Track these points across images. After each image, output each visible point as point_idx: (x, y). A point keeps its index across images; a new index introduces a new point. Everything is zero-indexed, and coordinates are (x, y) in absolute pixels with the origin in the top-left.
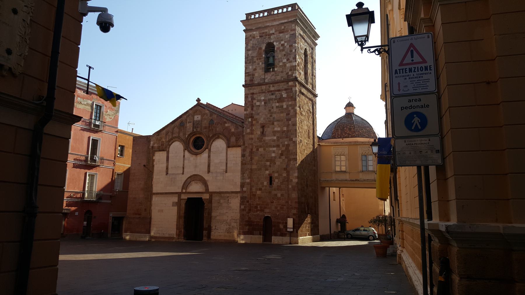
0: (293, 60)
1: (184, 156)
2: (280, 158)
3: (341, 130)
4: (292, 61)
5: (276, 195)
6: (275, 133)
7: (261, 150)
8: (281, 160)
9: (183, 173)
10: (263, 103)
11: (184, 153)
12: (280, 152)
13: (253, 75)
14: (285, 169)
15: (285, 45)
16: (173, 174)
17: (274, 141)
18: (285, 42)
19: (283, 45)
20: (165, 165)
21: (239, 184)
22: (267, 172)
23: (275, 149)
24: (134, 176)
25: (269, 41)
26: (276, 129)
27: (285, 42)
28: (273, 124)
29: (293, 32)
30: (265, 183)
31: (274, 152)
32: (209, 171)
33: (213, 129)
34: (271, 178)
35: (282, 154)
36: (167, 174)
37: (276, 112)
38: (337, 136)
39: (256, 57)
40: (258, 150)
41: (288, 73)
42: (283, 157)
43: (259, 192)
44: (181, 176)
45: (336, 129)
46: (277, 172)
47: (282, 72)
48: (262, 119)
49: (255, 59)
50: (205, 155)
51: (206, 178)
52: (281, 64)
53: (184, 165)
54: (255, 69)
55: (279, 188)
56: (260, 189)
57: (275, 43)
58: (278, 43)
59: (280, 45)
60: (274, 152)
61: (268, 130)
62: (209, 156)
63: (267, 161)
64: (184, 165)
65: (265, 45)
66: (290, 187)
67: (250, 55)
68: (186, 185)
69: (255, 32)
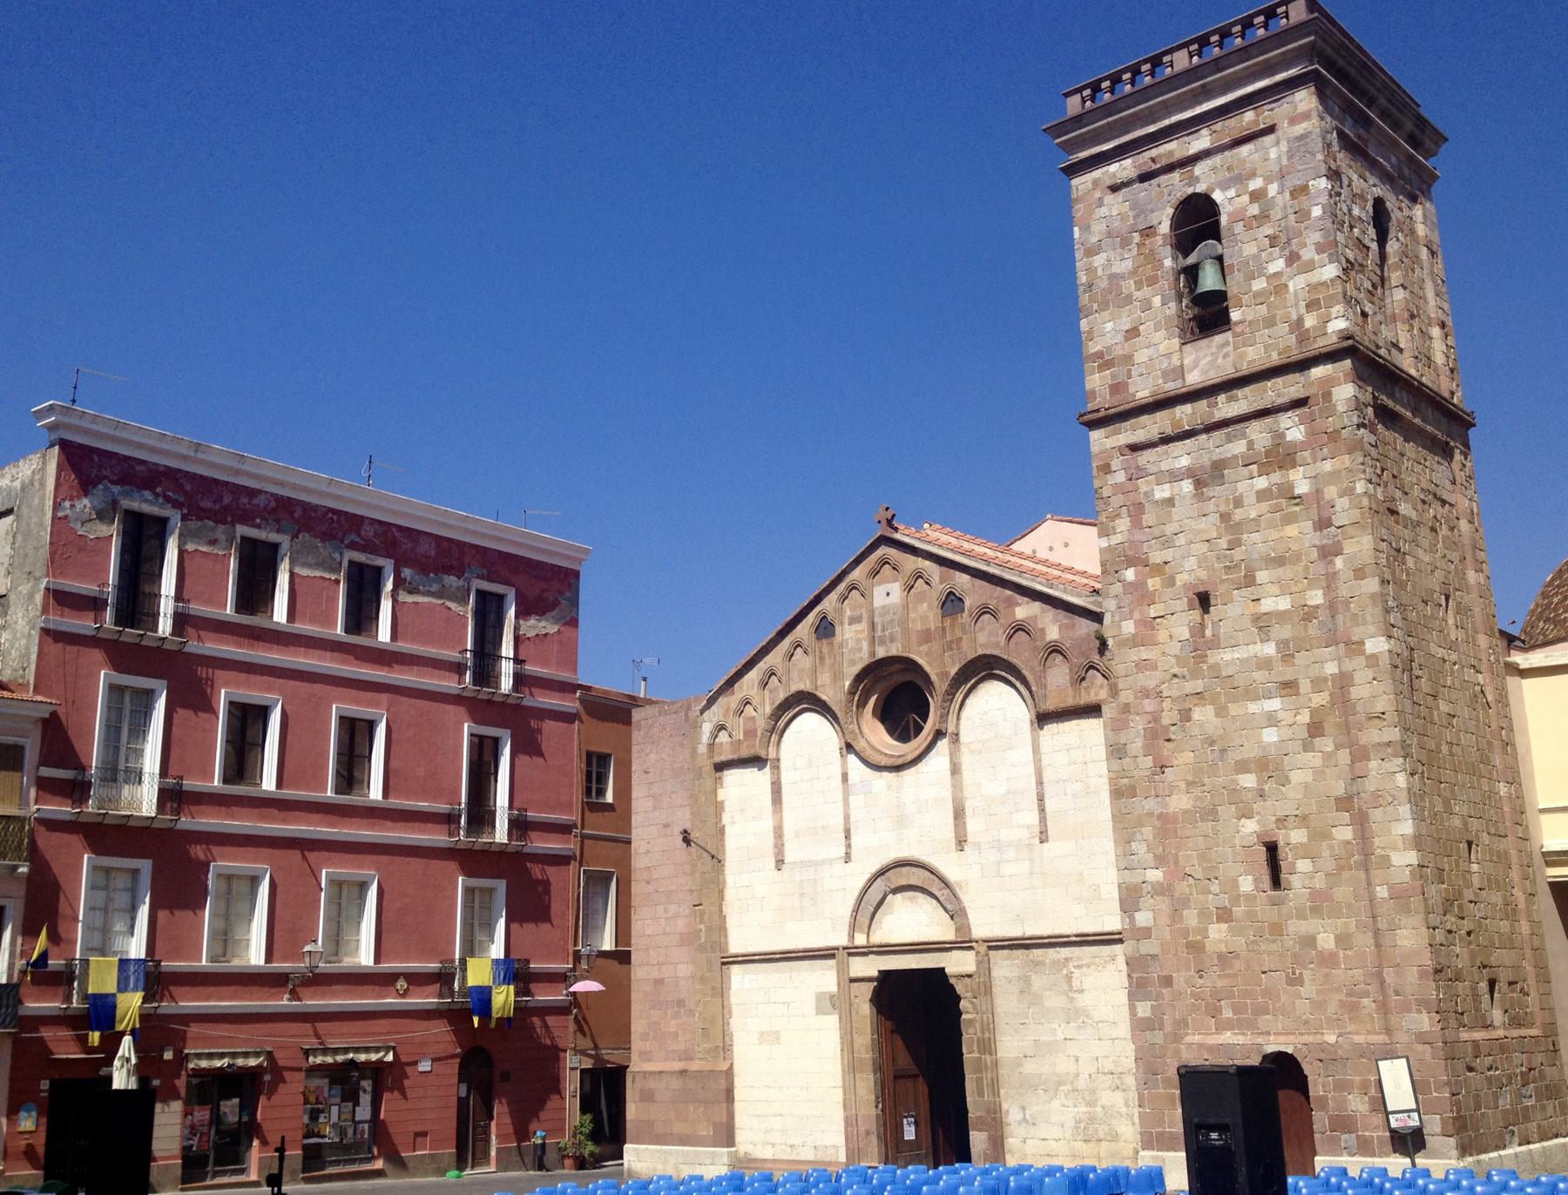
0: (1316, 257)
1: (845, 777)
2: (1308, 747)
4: (1312, 261)
5: (1310, 941)
6: (1263, 624)
7: (1203, 714)
8: (1315, 759)
9: (848, 858)
10: (1187, 486)
11: (844, 764)
12: (1304, 717)
13: (1128, 359)
14: (1344, 803)
16: (804, 864)
17: (1265, 664)
18: (1268, 180)
19: (1256, 196)
21: (1112, 894)
22: (1250, 826)
23: (1274, 704)
24: (648, 883)
25: (1190, 191)
26: (1267, 605)
27: (1268, 180)
28: (1250, 581)
29: (1304, 125)
30: (1246, 884)
31: (1272, 720)
32: (961, 843)
34: (1272, 849)
35: (1315, 729)
36: (780, 863)
37: (1256, 520)
39: (1134, 273)
40: (1186, 715)
41: (1300, 320)
43: (1217, 933)
44: (840, 867)
46: (1303, 820)
47: (1270, 322)
48: (1191, 563)
49: (1129, 285)
50: (939, 759)
51: (951, 874)
52: (1259, 285)
53: (847, 817)
54: (1133, 333)
55: (1320, 903)
56: (1224, 915)
57: (1217, 196)
58: (1232, 193)
59: (1246, 198)
60: (1272, 720)
61: (1231, 611)
62: (955, 770)
63: (1242, 767)
64: (847, 817)
65: (1170, 211)
66: (1382, 892)
67: (1100, 272)
68: (868, 907)
69: (1117, 164)
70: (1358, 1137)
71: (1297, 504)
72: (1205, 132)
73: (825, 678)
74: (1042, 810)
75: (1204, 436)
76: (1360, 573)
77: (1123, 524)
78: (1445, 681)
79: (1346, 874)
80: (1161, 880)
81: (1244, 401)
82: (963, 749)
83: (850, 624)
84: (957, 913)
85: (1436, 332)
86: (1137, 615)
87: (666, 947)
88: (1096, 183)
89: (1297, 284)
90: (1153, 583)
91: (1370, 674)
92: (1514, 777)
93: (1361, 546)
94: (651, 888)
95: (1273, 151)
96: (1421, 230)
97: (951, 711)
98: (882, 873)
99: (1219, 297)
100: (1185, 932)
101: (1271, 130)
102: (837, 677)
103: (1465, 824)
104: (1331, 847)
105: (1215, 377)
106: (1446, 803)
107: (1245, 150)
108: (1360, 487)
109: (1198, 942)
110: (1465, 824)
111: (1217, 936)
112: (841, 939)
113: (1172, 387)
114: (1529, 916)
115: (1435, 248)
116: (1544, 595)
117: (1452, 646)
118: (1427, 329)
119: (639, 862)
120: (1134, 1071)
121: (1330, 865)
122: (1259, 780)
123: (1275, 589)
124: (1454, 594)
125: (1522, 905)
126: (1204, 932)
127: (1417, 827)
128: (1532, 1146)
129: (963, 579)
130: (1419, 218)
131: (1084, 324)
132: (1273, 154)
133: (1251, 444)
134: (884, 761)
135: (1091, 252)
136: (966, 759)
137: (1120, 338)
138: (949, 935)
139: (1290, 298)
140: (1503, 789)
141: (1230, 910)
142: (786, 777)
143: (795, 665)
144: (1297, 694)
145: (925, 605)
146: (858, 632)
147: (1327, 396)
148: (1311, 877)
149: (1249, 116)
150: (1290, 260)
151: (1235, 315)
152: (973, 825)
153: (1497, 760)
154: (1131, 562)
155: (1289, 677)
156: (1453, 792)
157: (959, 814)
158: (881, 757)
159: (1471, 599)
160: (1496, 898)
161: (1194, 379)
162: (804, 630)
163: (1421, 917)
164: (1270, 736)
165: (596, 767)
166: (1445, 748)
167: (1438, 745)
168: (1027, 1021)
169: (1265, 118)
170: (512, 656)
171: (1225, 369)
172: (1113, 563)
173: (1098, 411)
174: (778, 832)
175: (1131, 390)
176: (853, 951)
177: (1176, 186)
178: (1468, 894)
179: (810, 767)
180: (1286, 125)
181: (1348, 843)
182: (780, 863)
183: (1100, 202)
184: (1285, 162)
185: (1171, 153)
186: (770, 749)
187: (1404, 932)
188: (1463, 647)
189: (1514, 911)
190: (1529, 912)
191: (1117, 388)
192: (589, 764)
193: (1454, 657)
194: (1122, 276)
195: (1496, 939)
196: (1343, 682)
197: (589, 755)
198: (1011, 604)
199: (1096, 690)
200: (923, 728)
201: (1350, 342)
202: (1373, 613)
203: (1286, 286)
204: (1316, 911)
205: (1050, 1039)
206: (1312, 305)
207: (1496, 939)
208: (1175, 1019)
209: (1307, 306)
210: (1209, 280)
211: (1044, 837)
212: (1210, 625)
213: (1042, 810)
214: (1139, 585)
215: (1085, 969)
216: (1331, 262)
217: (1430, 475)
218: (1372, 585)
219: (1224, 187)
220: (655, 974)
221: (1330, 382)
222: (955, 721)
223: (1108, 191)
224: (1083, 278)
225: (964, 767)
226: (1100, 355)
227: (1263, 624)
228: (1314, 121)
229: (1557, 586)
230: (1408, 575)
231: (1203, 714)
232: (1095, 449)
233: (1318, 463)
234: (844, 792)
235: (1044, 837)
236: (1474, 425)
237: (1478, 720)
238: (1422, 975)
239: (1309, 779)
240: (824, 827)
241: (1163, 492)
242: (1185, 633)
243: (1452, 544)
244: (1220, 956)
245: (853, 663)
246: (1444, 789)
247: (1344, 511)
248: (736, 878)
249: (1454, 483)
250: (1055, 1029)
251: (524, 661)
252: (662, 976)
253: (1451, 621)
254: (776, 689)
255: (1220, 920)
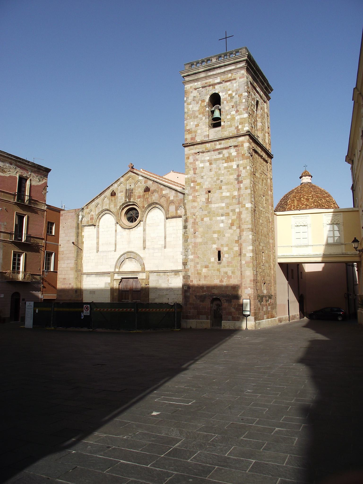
1: (116, 231)
2: (230, 228)
3: (298, 200)
5: (226, 273)
6: (222, 199)
7: (206, 219)
8: (231, 231)
9: (115, 251)
10: (208, 164)
11: (116, 228)
12: (230, 221)
13: (196, 132)
14: (237, 242)
15: (233, 95)
16: (103, 252)
17: (222, 208)
18: (233, 92)
19: (230, 95)
20: (95, 242)
21: (181, 261)
22: (215, 246)
23: (223, 218)
24: (63, 254)
26: (224, 194)
27: (233, 92)
28: (220, 188)
29: (243, 79)
30: (213, 259)
31: (222, 222)
32: (144, 248)
33: (148, 198)
34: (219, 253)
35: (232, 224)
36: (98, 251)
37: (223, 174)
38: (293, 208)
39: (199, 111)
40: (202, 220)
41: (238, 127)
42: (234, 228)
43: (204, 270)
44: (113, 253)
45: (292, 200)
46: (227, 245)
47: (231, 126)
48: (207, 183)
49: (197, 114)
50: (140, 228)
51: (142, 255)
52: (229, 117)
53: (116, 241)
54: (197, 125)
55: (229, 264)
56: (206, 267)
57: (220, 94)
58: (224, 94)
59: (227, 95)
60: (222, 222)
61: (215, 196)
62: (144, 230)
63: (214, 232)
64: (116, 241)
66: (243, 262)
67: (190, 109)
68: (121, 262)
70: (232, 317)
71: (233, 171)
72: (219, 78)
73: (112, 206)
74: (165, 241)
75: (213, 152)
76: (246, 188)
77: (192, 172)
78: (262, 215)
79: (236, 258)
80: (193, 258)
81: (224, 144)
82: (147, 225)
83: (120, 193)
84: (143, 265)
85: (267, 135)
86: (193, 195)
87: (67, 270)
88: (191, 87)
89: (238, 118)
90: (197, 187)
91: (246, 212)
92: (274, 239)
93: (247, 182)
94: (63, 256)
95: (235, 85)
96: (266, 110)
97: (144, 216)
98: (124, 254)
99: (219, 119)
100: (197, 270)
101: (235, 79)
102: (115, 206)
103: (263, 248)
104: (233, 252)
105: (216, 138)
106: (259, 243)
107: (228, 83)
108: (248, 168)
109: (200, 272)
110: (263, 248)
111: (204, 271)
112: (112, 270)
113: (206, 139)
114: (273, 270)
115: (268, 115)
116: (281, 201)
117: (264, 208)
118: (265, 134)
119: (61, 249)
120: (182, 302)
121: (233, 256)
122: (218, 235)
123: (226, 191)
124: (266, 196)
125: (272, 267)
126: (202, 270)
127: (253, 248)
128: (269, 319)
129: (150, 182)
130: (265, 106)
131: (185, 122)
132: (235, 85)
133: (224, 155)
134: (128, 227)
135: (188, 104)
136: (147, 228)
137: (194, 126)
138: (140, 270)
139: (236, 121)
140: (271, 241)
141: (208, 265)
142: (100, 230)
143: (105, 202)
144: (229, 216)
145: (140, 189)
146: (122, 195)
147: (242, 145)
148: (227, 258)
149: (230, 75)
150: (237, 111)
151: (222, 123)
152: (148, 244)
153: (270, 234)
154: (193, 182)
155: (227, 212)
156: (261, 240)
157: (144, 241)
158: (125, 226)
159: (269, 198)
160: (267, 265)
161: (211, 138)
162: (108, 193)
163: (252, 268)
164: (222, 225)
165: (50, 225)
166: (260, 231)
167: (259, 230)
168: (157, 290)
169: (233, 76)
170: (28, 195)
171: (219, 136)
172: (188, 181)
173: (187, 144)
174: (98, 243)
175: (196, 139)
176: (114, 273)
177: (212, 91)
178: (262, 264)
179: (107, 228)
180: (238, 78)
181: (237, 251)
182: (98, 251)
183: (192, 92)
184: (237, 88)
185: (210, 82)
186: (97, 223)
187: (248, 271)
188: (266, 208)
189: (271, 268)
190: (274, 269)
191: (192, 139)
192: (48, 225)
193: (264, 210)
194: (196, 111)
195: (266, 274)
196: (240, 213)
197: (49, 222)
198: (162, 190)
199: (181, 212)
200: (137, 220)
201: (249, 133)
202: (248, 198)
203: (235, 118)
204: (228, 266)
205: (162, 294)
206: (241, 123)
207: (266, 274)
208: (193, 290)
209: (240, 123)
210: (217, 114)
211: (165, 247)
212: (210, 198)
213: (165, 241)
214: (194, 187)
215: (172, 279)
216: (246, 113)
217: (263, 168)
218: (249, 191)
219: (222, 92)
220: (63, 277)
221: (243, 142)
222: (145, 218)
223: (194, 90)
224: (186, 110)
225: (146, 230)
226: (189, 130)
227: (222, 199)
228: (245, 78)
229: (284, 200)
230: (256, 190)
231: (206, 219)
232: (186, 153)
233: (239, 161)
234: (115, 235)
235: (165, 247)
236: (273, 158)
237: (267, 225)
238: (251, 281)
239: (230, 236)
240: (109, 243)
241: (201, 165)
242: (204, 200)
243: (266, 184)
244: (205, 276)
245: (120, 202)
246: (259, 240)
247: (244, 173)
248: (85, 254)
249: (268, 170)
250: (164, 292)
251: (32, 197)
252: (65, 277)
253: (264, 202)
254: (99, 208)
255: (205, 268)
